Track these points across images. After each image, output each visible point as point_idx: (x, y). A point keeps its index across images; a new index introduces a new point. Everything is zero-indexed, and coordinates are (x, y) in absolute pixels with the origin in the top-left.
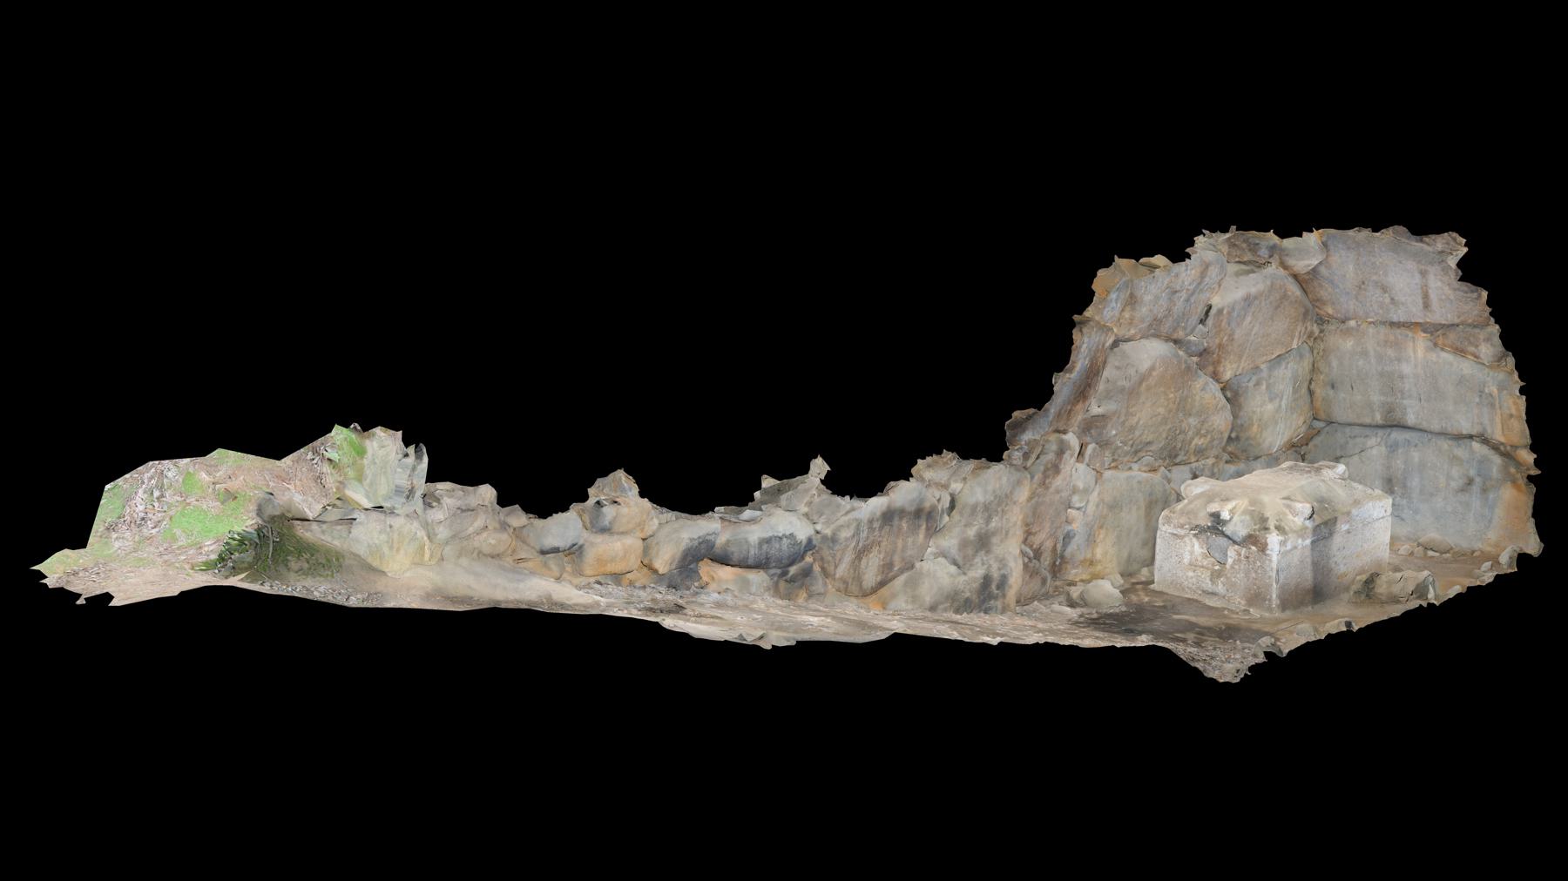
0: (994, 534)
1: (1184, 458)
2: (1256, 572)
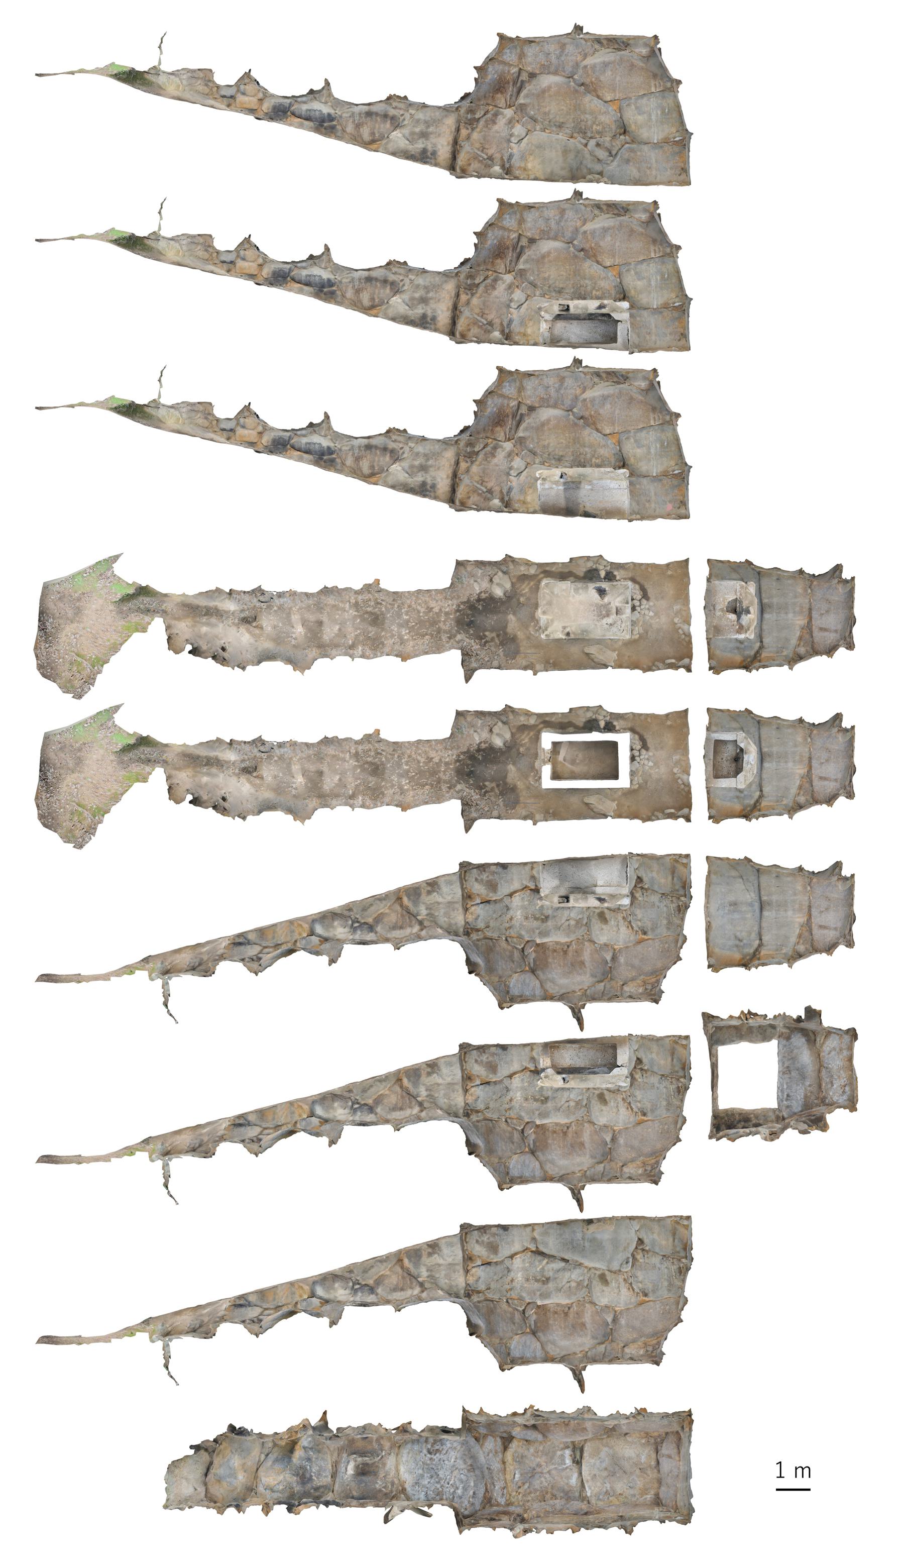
0: (431, 466)
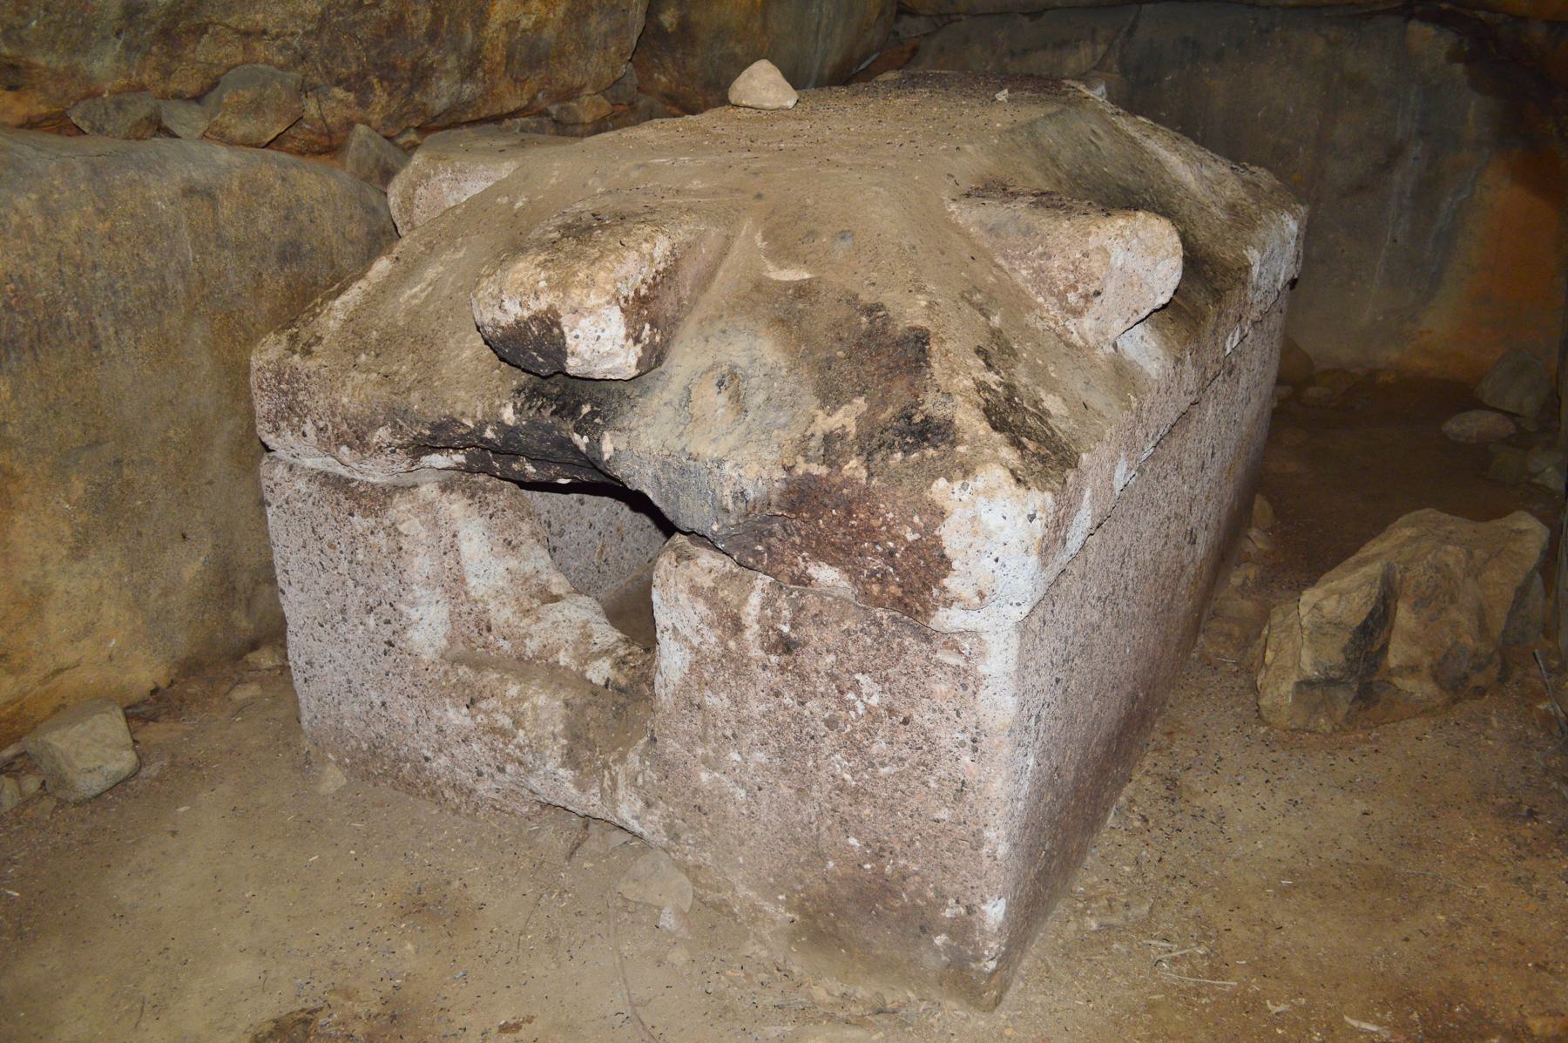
1: (468, 89)
2: (854, 747)
